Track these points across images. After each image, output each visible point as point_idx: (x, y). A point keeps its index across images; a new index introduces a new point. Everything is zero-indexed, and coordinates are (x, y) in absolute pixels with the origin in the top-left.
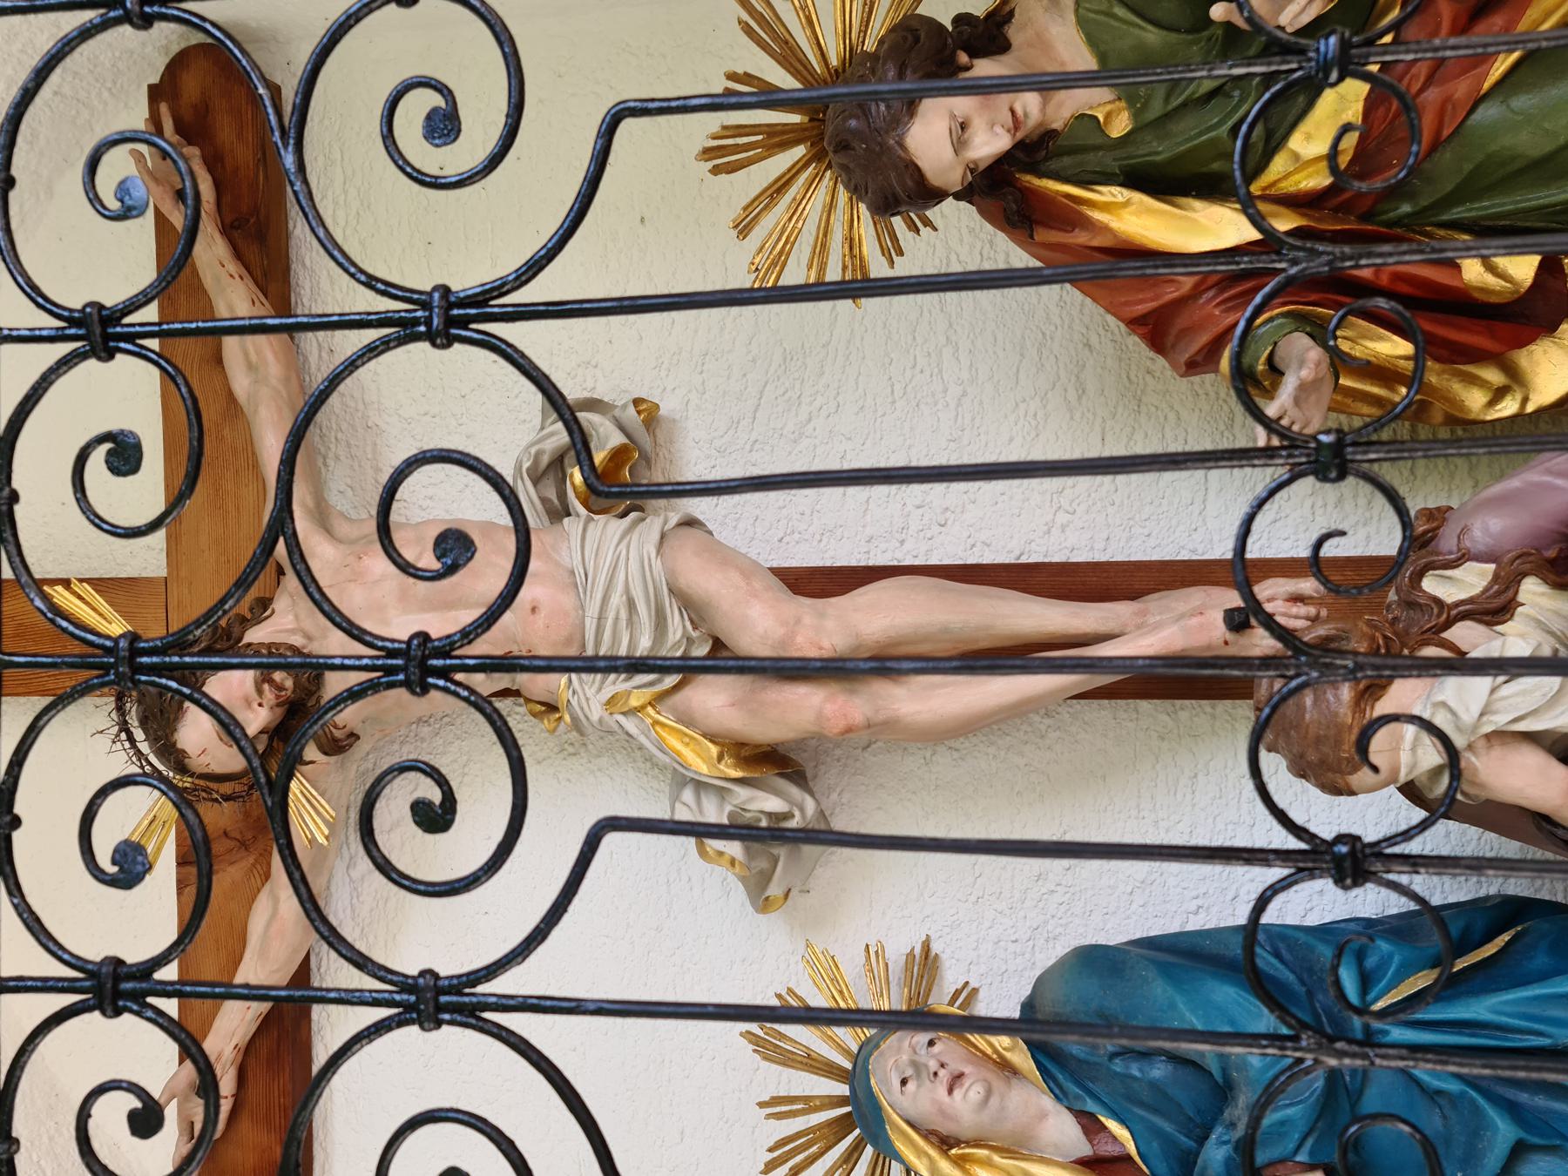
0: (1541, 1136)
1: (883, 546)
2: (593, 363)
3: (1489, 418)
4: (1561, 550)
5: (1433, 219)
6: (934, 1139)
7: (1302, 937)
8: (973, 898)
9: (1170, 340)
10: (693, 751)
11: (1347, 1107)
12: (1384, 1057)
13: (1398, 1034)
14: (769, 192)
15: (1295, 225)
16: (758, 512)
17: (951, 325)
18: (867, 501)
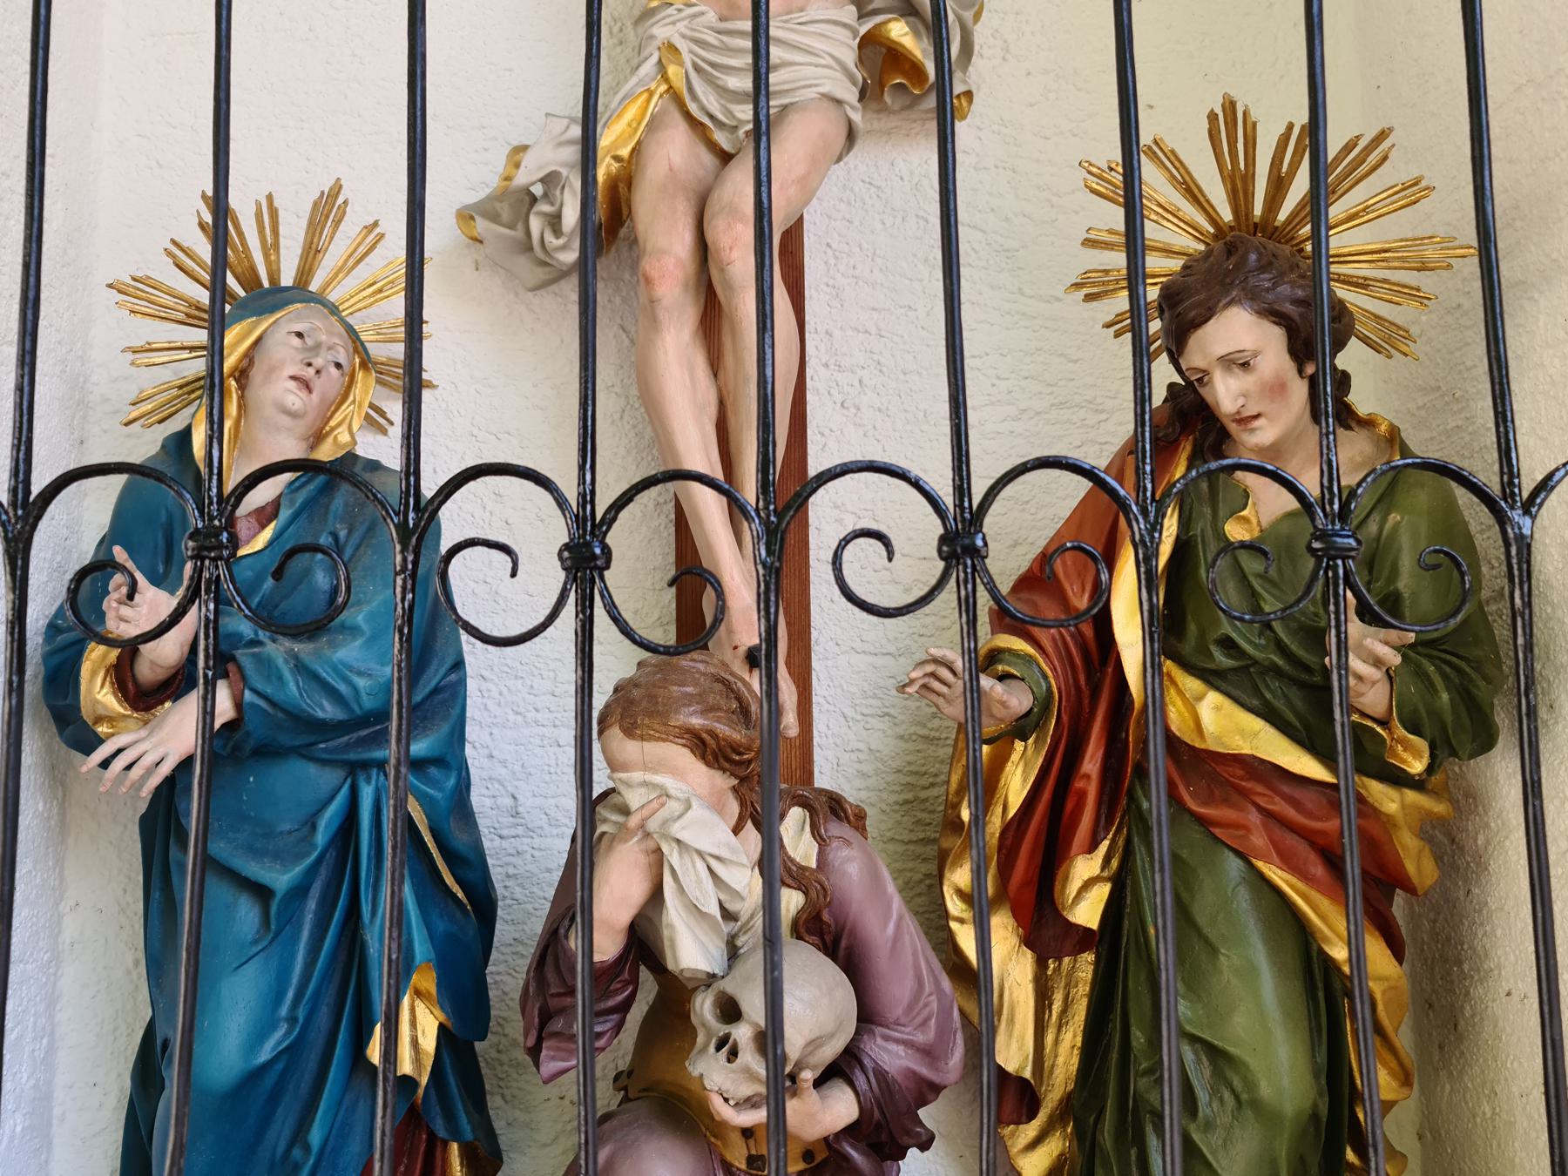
0: (279, 913)
1: (822, 347)
2: (1008, 56)
3: (945, 888)
4: (829, 926)
5: (1134, 828)
6: (245, 363)
7: (455, 712)
8: (476, 432)
9: (1025, 595)
10: (623, 132)
11: (297, 743)
12: (404, 581)
13: (367, 794)
14: (1188, 179)
15: (1135, 695)
16: (856, 223)
17: (1037, 413)
18: (866, 332)
